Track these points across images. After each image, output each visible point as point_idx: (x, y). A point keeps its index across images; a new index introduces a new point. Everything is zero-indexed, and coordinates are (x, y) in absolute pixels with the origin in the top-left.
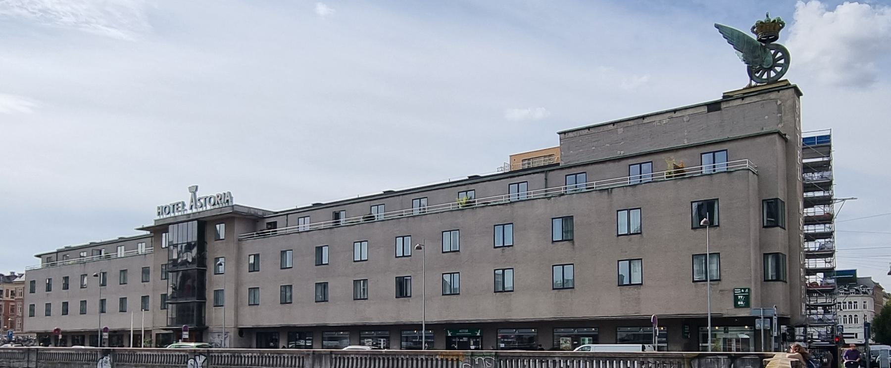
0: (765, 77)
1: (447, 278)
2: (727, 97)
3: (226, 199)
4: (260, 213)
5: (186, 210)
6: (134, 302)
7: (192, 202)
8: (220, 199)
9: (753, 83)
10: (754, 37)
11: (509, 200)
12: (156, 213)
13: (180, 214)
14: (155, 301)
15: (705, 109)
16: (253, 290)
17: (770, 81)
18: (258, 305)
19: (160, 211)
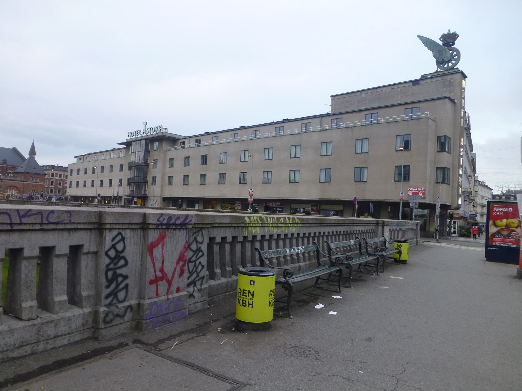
0: (446, 66)
1: (266, 176)
2: (424, 77)
3: (160, 129)
4: (177, 137)
5: (141, 134)
6: (116, 182)
7: (144, 130)
8: (157, 129)
9: (439, 70)
10: (441, 43)
13: (138, 136)
14: (125, 182)
15: (411, 84)
16: (171, 177)
17: (449, 69)
18: (172, 185)
19: (129, 134)
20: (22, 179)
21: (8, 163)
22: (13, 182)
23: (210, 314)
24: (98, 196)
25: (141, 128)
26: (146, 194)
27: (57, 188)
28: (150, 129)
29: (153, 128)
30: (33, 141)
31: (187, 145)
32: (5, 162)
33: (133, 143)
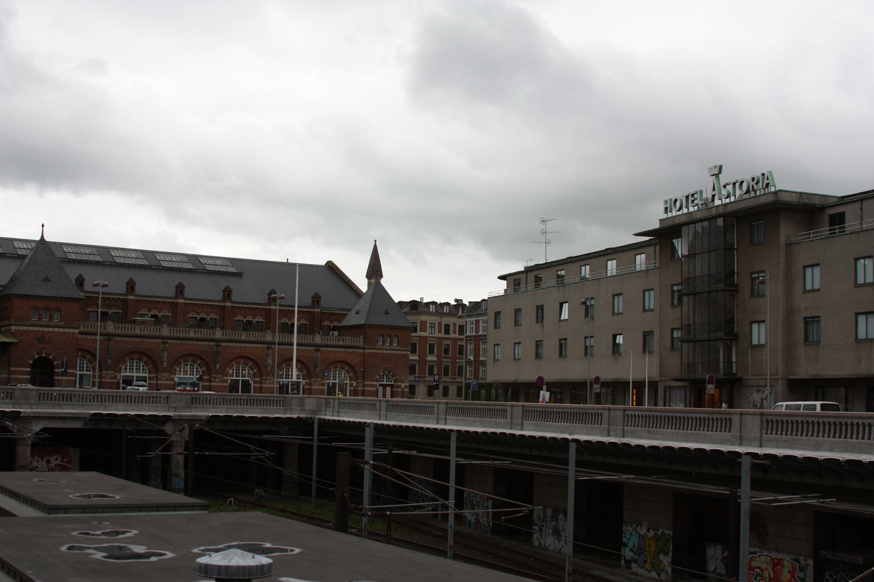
3: (766, 181)
7: (714, 189)
8: (757, 183)
11: (526, 289)
12: (663, 210)
19: (668, 205)
20: (361, 344)
21: (323, 303)
22: (339, 352)
23: (386, 511)
24: (595, 383)
25: (705, 185)
26: (734, 372)
27: (426, 361)
28: (734, 184)
29: (742, 182)
30: (375, 241)
31: (851, 224)
32: (318, 302)
33: (684, 229)
